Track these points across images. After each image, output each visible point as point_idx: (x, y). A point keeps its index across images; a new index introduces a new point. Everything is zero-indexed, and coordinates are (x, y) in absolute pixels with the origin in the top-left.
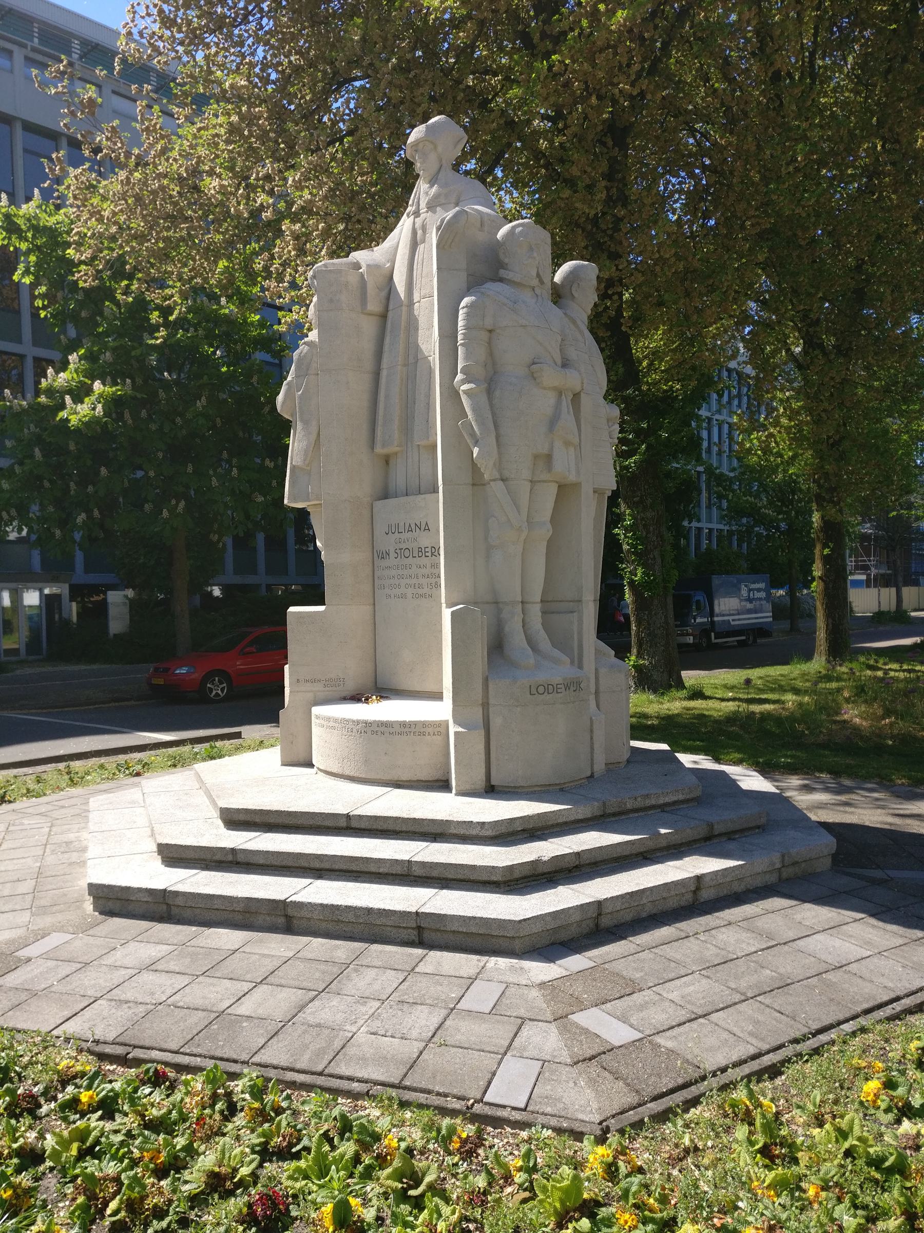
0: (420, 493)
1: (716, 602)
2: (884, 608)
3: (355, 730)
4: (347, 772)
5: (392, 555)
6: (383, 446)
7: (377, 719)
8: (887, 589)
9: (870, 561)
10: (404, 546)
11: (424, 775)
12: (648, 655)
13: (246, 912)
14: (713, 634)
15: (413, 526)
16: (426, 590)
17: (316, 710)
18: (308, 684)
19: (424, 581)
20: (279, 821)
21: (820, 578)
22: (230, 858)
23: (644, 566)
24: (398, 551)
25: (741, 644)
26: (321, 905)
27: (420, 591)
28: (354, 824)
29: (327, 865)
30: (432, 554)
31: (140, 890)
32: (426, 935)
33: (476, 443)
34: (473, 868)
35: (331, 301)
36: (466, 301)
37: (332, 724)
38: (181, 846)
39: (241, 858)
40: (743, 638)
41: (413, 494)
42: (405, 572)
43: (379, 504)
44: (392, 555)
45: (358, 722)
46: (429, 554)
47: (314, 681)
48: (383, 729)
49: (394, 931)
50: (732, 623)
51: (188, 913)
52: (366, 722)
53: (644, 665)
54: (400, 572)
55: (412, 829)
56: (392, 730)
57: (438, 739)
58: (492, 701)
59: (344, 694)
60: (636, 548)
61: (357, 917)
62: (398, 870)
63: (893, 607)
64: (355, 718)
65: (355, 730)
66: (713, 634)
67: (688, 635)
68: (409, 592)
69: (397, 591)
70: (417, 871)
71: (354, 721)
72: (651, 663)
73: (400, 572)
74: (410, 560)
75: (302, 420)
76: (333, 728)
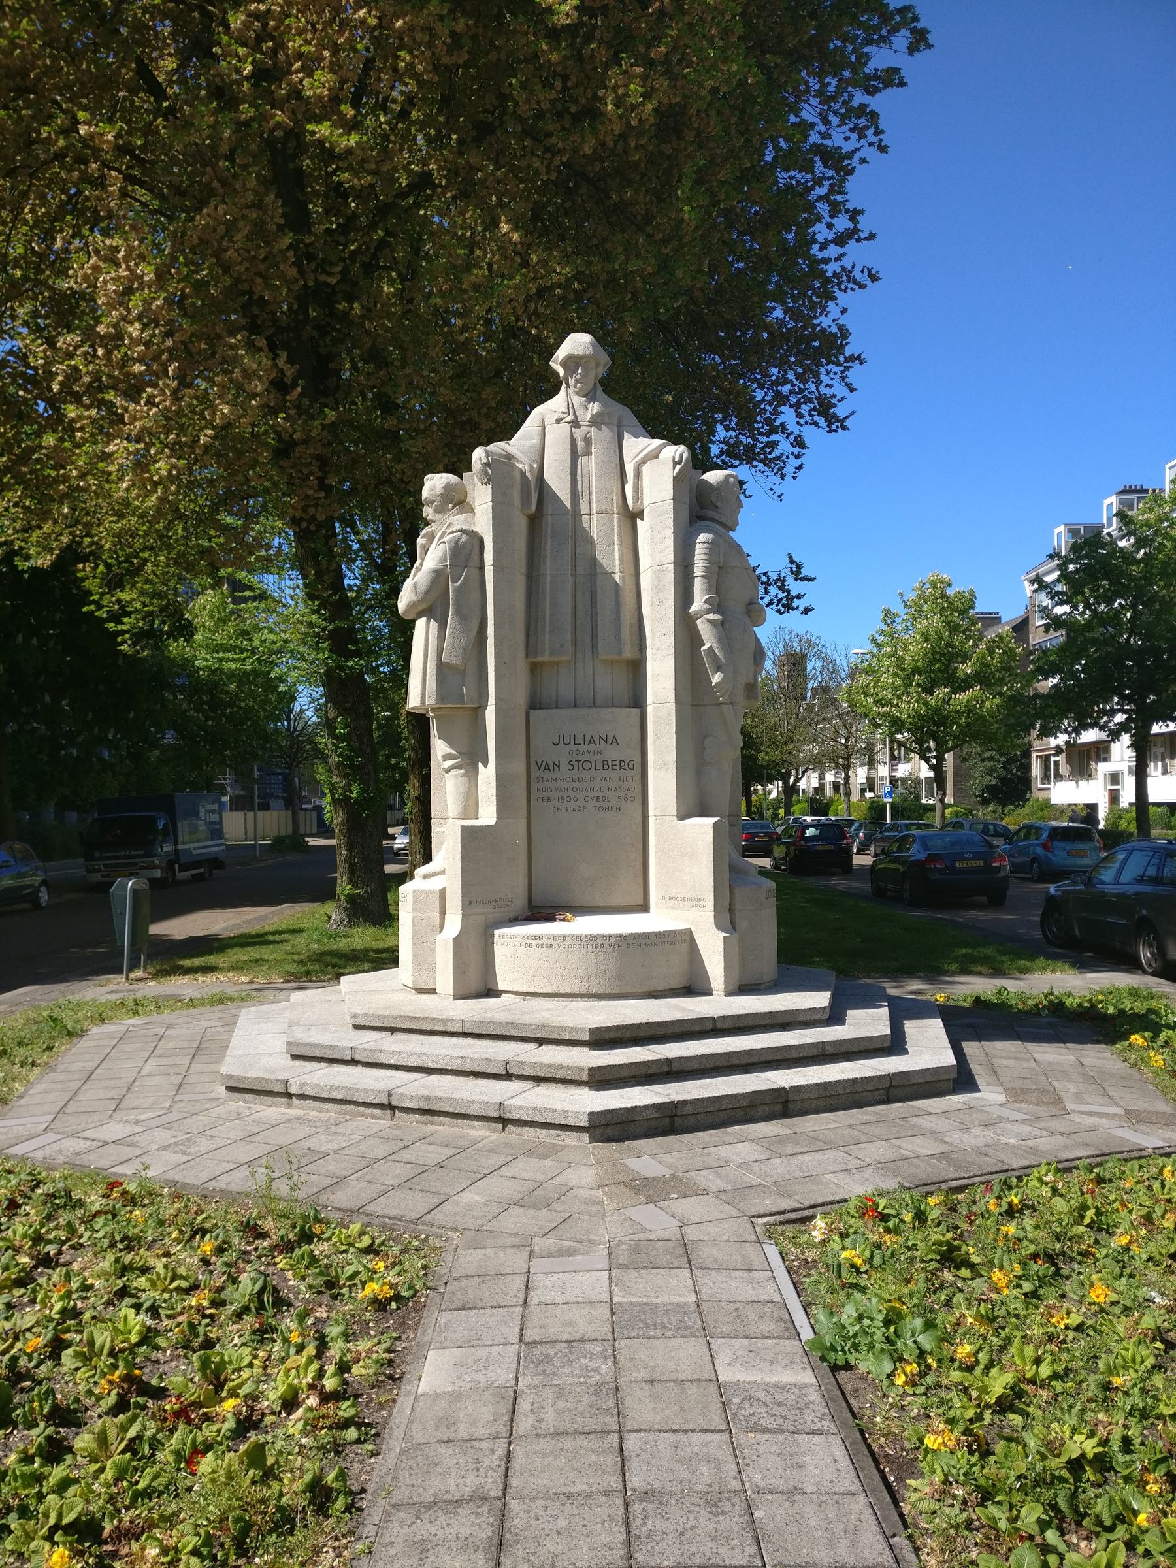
0: (594, 705)
1: (179, 824)
2: (283, 833)
3: (606, 945)
4: (594, 990)
5: (564, 766)
6: (551, 654)
7: (634, 931)
8: (240, 815)
9: (225, 779)
10: (583, 758)
11: (675, 983)
12: (363, 882)
13: (752, 1106)
14: (177, 866)
15: (596, 739)
16: (612, 803)
17: (497, 932)
18: (480, 906)
19: (611, 794)
20: (650, 1032)
21: (416, 798)
22: (665, 1069)
23: (361, 781)
24: (575, 764)
25: (197, 878)
26: (817, 1084)
27: (605, 804)
28: (719, 1025)
29: (755, 1059)
30: (621, 768)
31: (647, 1107)
32: (892, 1092)
33: (718, 669)
34: (871, 1039)
35: (504, 494)
36: (703, 537)
37: (567, 942)
38: (615, 1066)
39: (676, 1067)
40: (202, 870)
41: (584, 706)
42: (585, 785)
43: (532, 712)
44: (564, 766)
45: (610, 936)
46: (618, 768)
47: (485, 902)
48: (640, 941)
49: (869, 1095)
50: (194, 852)
51: (691, 1121)
52: (620, 936)
53: (358, 894)
54: (577, 784)
55: (768, 1022)
56: (648, 941)
57: (684, 948)
58: (738, 906)
59: (512, 915)
60: (352, 761)
61: (845, 1088)
62: (814, 1052)
63: (290, 831)
64: (607, 932)
65: (606, 945)
66: (177, 866)
67: (155, 867)
68: (590, 805)
69: (573, 804)
70: (830, 1050)
71: (604, 936)
72: (366, 892)
73: (577, 784)
74: (592, 772)
75: (458, 613)
76: (574, 946)
